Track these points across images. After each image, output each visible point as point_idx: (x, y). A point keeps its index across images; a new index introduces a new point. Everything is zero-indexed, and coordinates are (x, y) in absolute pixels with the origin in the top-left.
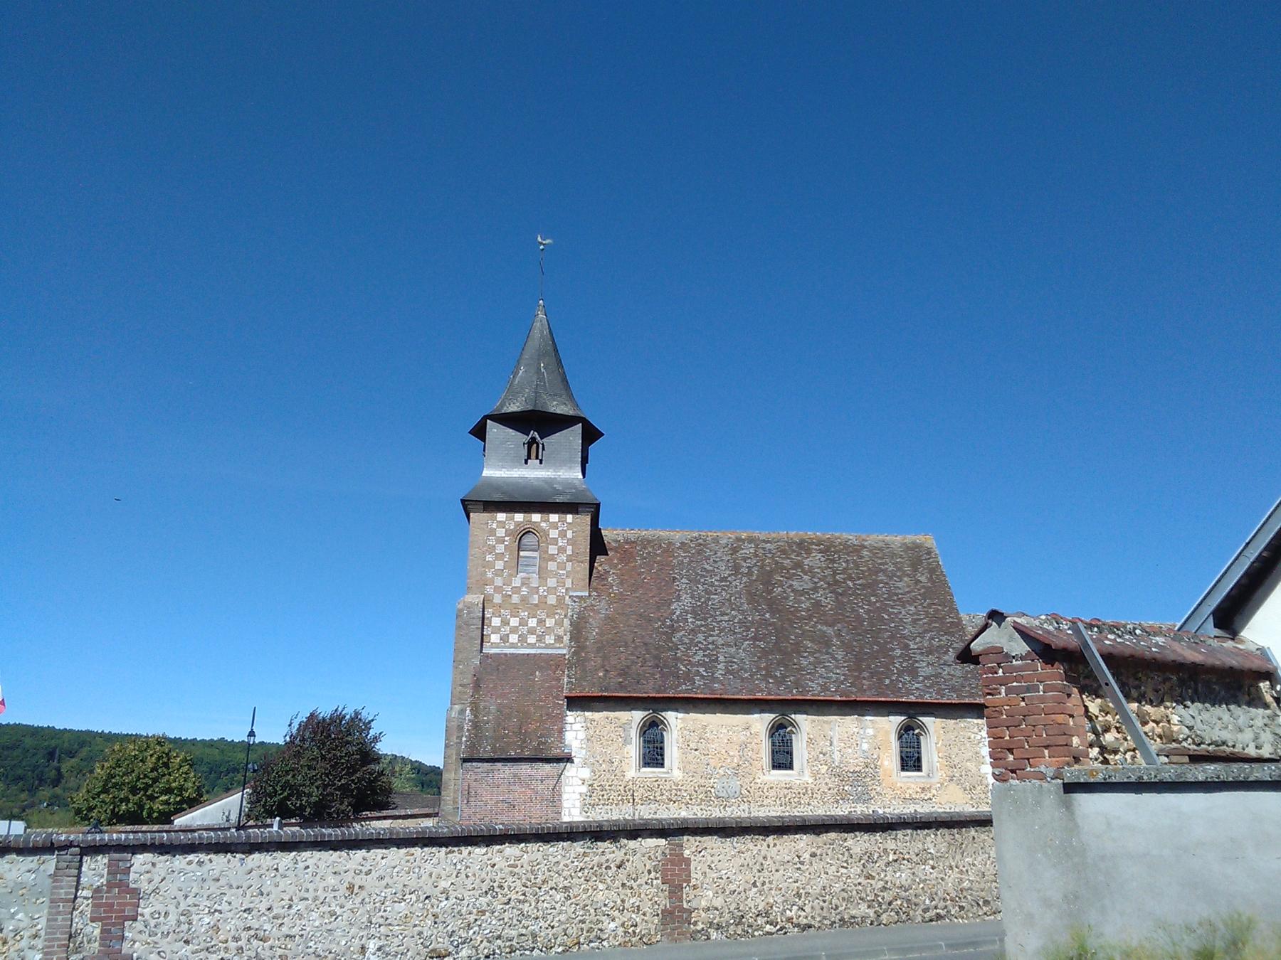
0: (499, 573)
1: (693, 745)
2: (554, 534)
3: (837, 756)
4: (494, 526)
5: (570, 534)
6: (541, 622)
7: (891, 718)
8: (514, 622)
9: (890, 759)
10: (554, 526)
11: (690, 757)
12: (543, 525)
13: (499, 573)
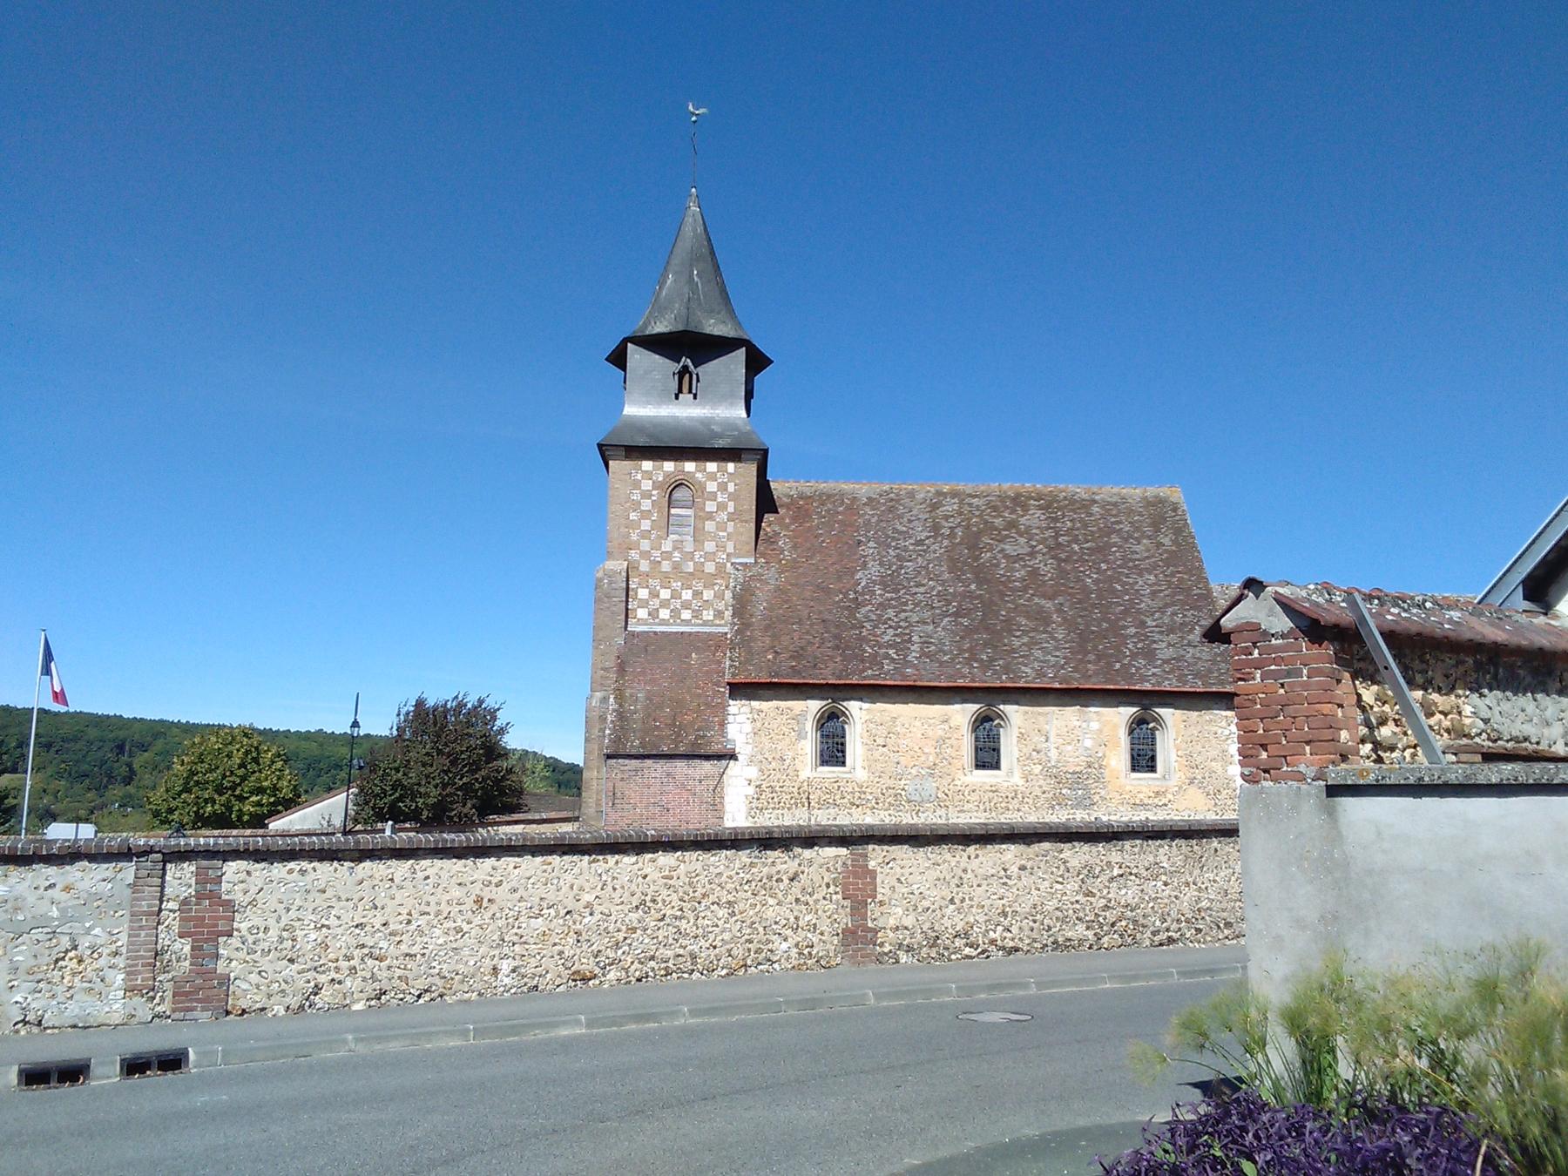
0: (645, 535)
1: (880, 741)
2: (712, 487)
3: (1053, 754)
4: (639, 477)
5: (731, 487)
6: (697, 594)
7: (1122, 709)
8: (665, 594)
9: (1119, 758)
10: (712, 477)
11: (877, 755)
12: (699, 475)
13: (645, 535)
